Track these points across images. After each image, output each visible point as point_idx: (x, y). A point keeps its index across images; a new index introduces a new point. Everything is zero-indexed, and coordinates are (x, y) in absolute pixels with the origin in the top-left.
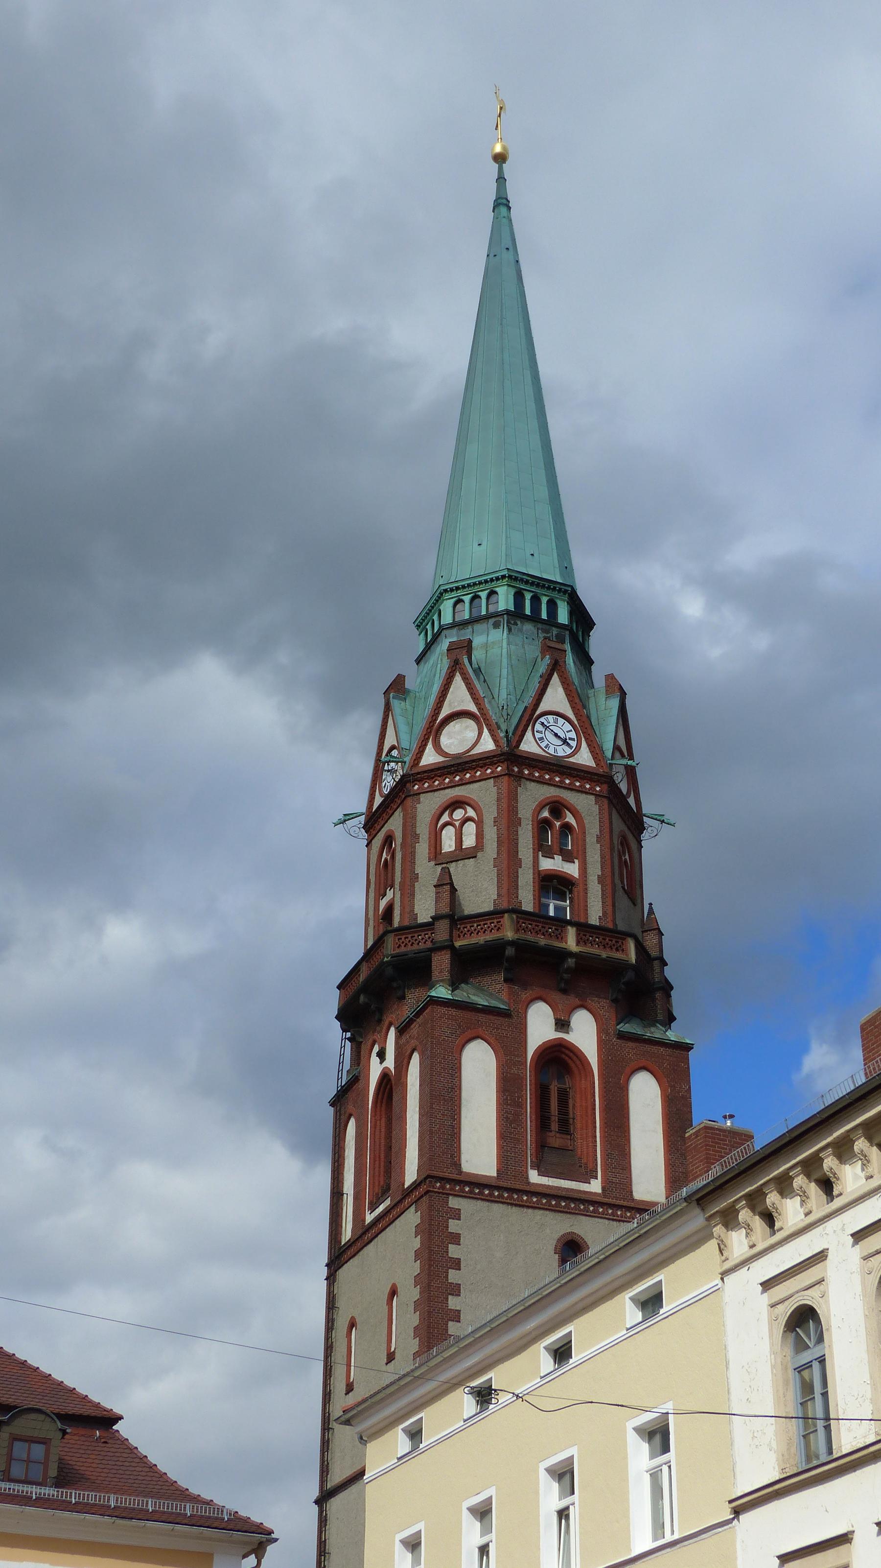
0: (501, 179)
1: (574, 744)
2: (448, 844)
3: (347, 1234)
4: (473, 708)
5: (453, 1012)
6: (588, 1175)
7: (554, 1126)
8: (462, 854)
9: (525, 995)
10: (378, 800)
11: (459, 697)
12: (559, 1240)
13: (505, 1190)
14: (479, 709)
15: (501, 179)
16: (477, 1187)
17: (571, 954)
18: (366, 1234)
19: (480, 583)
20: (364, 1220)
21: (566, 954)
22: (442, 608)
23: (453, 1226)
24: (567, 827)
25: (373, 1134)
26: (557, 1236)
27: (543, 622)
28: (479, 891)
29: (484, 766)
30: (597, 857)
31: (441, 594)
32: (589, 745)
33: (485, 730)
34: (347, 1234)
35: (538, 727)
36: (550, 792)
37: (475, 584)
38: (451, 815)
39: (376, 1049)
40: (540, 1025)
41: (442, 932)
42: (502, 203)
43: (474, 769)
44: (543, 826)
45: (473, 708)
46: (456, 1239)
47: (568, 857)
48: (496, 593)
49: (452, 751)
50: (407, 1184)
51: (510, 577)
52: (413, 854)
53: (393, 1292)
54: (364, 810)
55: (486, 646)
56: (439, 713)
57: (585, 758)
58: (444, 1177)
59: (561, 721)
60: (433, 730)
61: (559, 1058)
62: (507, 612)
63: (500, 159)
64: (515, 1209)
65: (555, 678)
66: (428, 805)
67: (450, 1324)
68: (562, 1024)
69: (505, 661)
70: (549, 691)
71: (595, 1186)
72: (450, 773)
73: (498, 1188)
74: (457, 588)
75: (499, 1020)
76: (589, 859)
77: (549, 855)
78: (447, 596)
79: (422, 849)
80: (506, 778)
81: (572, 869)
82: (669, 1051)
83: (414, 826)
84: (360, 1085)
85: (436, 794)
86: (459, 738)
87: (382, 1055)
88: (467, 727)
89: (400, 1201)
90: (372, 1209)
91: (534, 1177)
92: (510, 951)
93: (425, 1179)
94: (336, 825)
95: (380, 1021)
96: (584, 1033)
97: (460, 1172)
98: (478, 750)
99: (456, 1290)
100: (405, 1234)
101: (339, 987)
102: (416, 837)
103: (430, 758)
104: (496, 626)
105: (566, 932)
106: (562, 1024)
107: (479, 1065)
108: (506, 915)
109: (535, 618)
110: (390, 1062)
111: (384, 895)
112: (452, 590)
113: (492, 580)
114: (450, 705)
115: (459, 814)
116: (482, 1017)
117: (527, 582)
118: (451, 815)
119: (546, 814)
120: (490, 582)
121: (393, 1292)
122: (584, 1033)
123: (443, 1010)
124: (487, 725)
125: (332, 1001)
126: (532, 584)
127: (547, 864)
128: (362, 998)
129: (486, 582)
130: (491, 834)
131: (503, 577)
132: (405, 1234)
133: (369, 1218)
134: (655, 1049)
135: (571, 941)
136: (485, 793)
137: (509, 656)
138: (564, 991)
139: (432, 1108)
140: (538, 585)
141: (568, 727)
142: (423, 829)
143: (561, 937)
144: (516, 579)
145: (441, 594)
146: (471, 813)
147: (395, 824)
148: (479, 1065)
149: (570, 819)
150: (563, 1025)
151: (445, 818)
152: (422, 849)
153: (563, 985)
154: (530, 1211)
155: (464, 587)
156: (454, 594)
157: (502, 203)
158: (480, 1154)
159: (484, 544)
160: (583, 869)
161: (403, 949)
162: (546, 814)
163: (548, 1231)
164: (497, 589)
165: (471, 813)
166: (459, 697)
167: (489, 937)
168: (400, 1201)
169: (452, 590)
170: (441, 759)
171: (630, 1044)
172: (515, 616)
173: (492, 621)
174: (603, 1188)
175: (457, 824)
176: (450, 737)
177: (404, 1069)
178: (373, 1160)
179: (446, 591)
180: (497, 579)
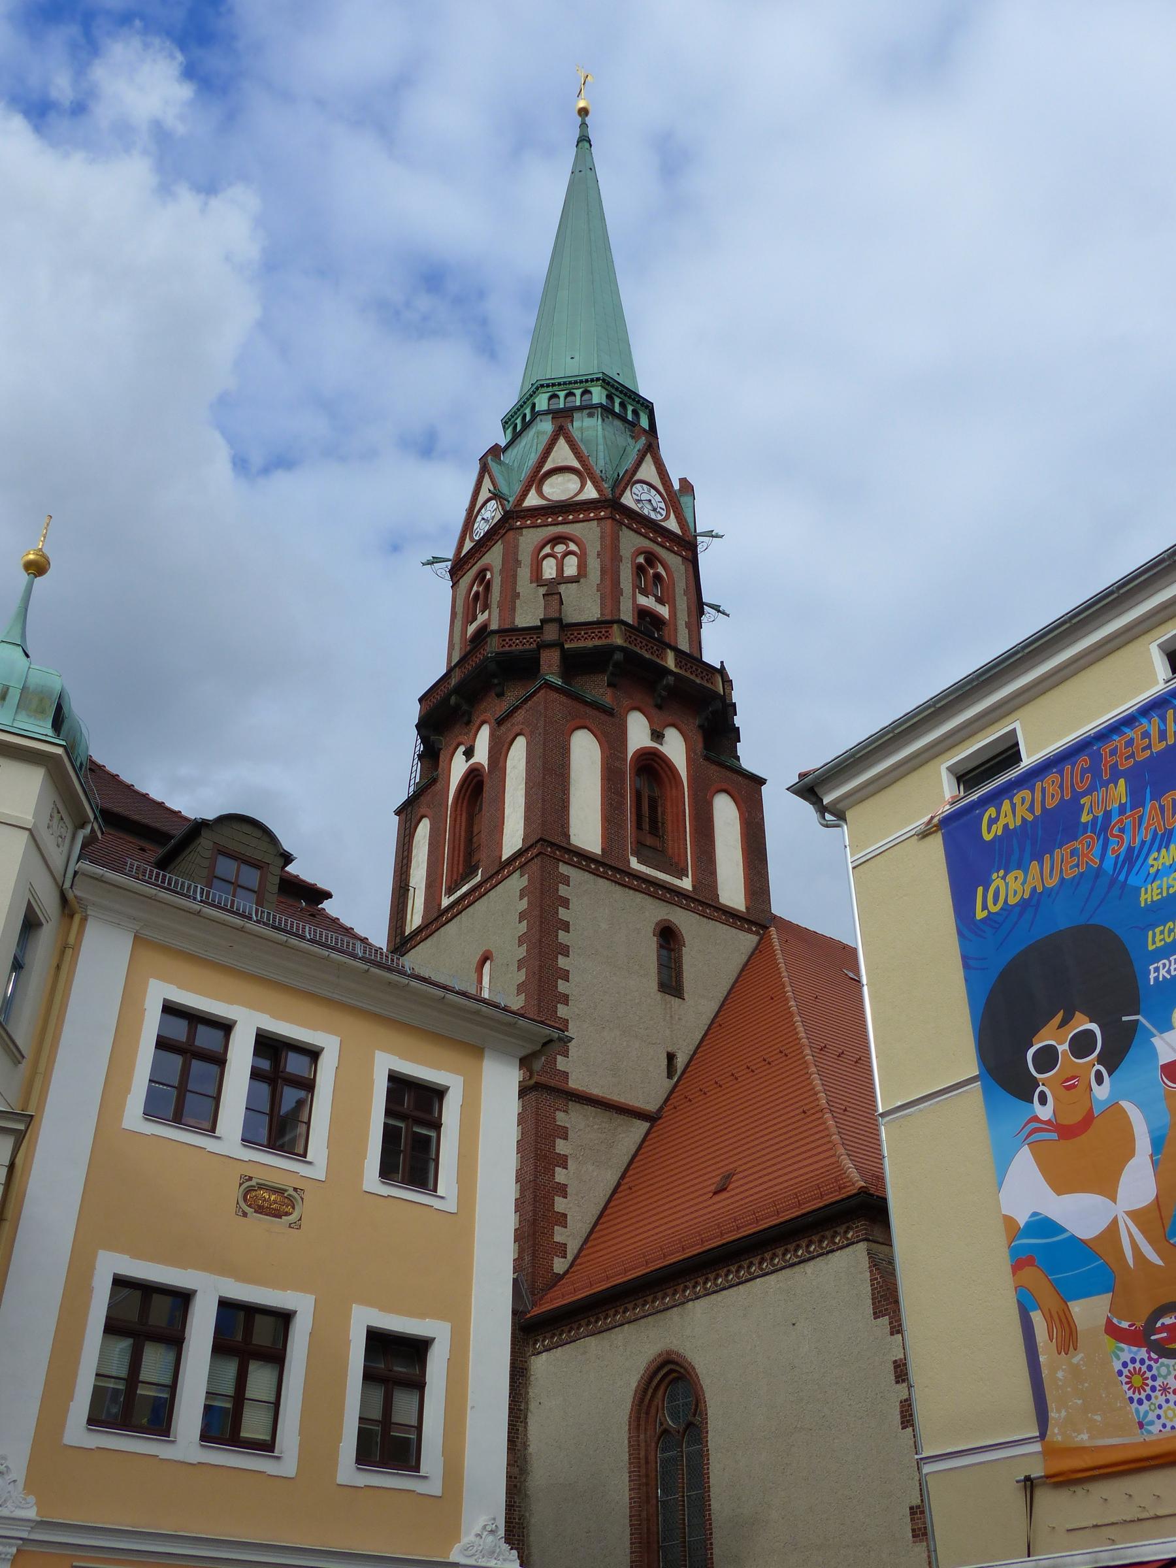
0: (584, 125)
1: (664, 513)
2: (549, 570)
3: (415, 918)
4: (576, 464)
5: (563, 699)
6: (681, 873)
7: (646, 826)
8: (561, 579)
9: (626, 703)
10: (468, 545)
11: (562, 454)
12: (657, 924)
13: (604, 866)
14: (583, 466)
15: (584, 125)
16: (583, 859)
17: (671, 672)
18: (436, 919)
19: (576, 382)
20: (440, 905)
21: (667, 671)
22: (536, 401)
23: (563, 890)
24: (657, 577)
25: (453, 827)
26: (656, 920)
27: (730, 916)
28: (583, 605)
29: (588, 510)
30: (685, 606)
31: (537, 389)
32: (676, 517)
33: (589, 482)
34: (415, 918)
35: (634, 489)
36: (647, 544)
37: (570, 383)
38: (552, 548)
39: (462, 749)
40: (638, 733)
41: (551, 633)
42: (584, 140)
43: (578, 511)
44: (640, 570)
45: (576, 464)
46: (565, 903)
47: (660, 601)
48: (590, 392)
49: (555, 497)
50: (504, 858)
51: (604, 380)
52: (515, 576)
53: (486, 958)
54: (450, 554)
55: (581, 429)
56: (542, 467)
57: (672, 525)
58: (549, 843)
59: (653, 492)
60: (537, 478)
61: (652, 765)
62: (601, 406)
63: (584, 112)
64: (618, 887)
65: (649, 457)
66: (529, 539)
67: (560, 981)
68: (657, 736)
69: (601, 441)
70: (644, 465)
71: (686, 884)
72: (553, 514)
73: (604, 864)
74: (553, 385)
75: (603, 717)
76: (678, 606)
77: (645, 593)
78: (545, 389)
79: (524, 573)
80: (610, 521)
81: (664, 611)
82: (746, 781)
83: (516, 553)
84: (438, 786)
85: (539, 529)
86: (560, 489)
87: (469, 754)
88: (569, 481)
89: (491, 877)
90: (450, 892)
91: (634, 863)
92: (618, 656)
93: (537, 842)
94: (424, 564)
95: (468, 723)
96: (675, 748)
97: (569, 844)
98: (582, 497)
99: (565, 951)
100: (509, 899)
101: (420, 700)
102: (518, 563)
103: (532, 500)
104: (590, 415)
105: (666, 654)
106: (657, 736)
107: (585, 753)
108: (615, 626)
109: (624, 419)
110: (481, 755)
111: (475, 619)
112: (548, 386)
113: (587, 381)
114: (553, 461)
115: (560, 548)
116: (588, 710)
117: (617, 389)
118: (552, 548)
119: (641, 560)
120: (585, 383)
121: (486, 958)
122: (675, 748)
123: (556, 695)
124: (591, 479)
125: (413, 712)
126: (621, 392)
127: (643, 601)
128: (453, 700)
129: (581, 382)
130: (594, 565)
131: (598, 379)
132: (509, 899)
133: (446, 902)
134: (735, 776)
135: (670, 662)
136: (589, 532)
137: (604, 437)
138: (659, 707)
139: (544, 778)
140: (625, 395)
141: (658, 498)
142: (525, 556)
143: (662, 656)
144: (608, 384)
145: (537, 389)
146: (573, 547)
147: (494, 557)
148: (585, 753)
149: (661, 570)
150: (658, 737)
151: (547, 550)
152: (524, 573)
153: (659, 701)
154: (631, 892)
155: (559, 384)
156: (550, 389)
157: (584, 140)
158: (586, 828)
159: (577, 358)
160: (673, 612)
161: (507, 648)
162: (641, 560)
163: (647, 914)
164: (592, 389)
165: (573, 547)
166: (562, 454)
167: (597, 642)
168: (491, 877)
169: (548, 386)
170: (544, 502)
171: (714, 767)
172: (607, 411)
173: (586, 412)
174: (694, 886)
175: (559, 556)
176: (552, 486)
177: (505, 748)
178: (453, 849)
179: (542, 386)
180: (592, 380)
